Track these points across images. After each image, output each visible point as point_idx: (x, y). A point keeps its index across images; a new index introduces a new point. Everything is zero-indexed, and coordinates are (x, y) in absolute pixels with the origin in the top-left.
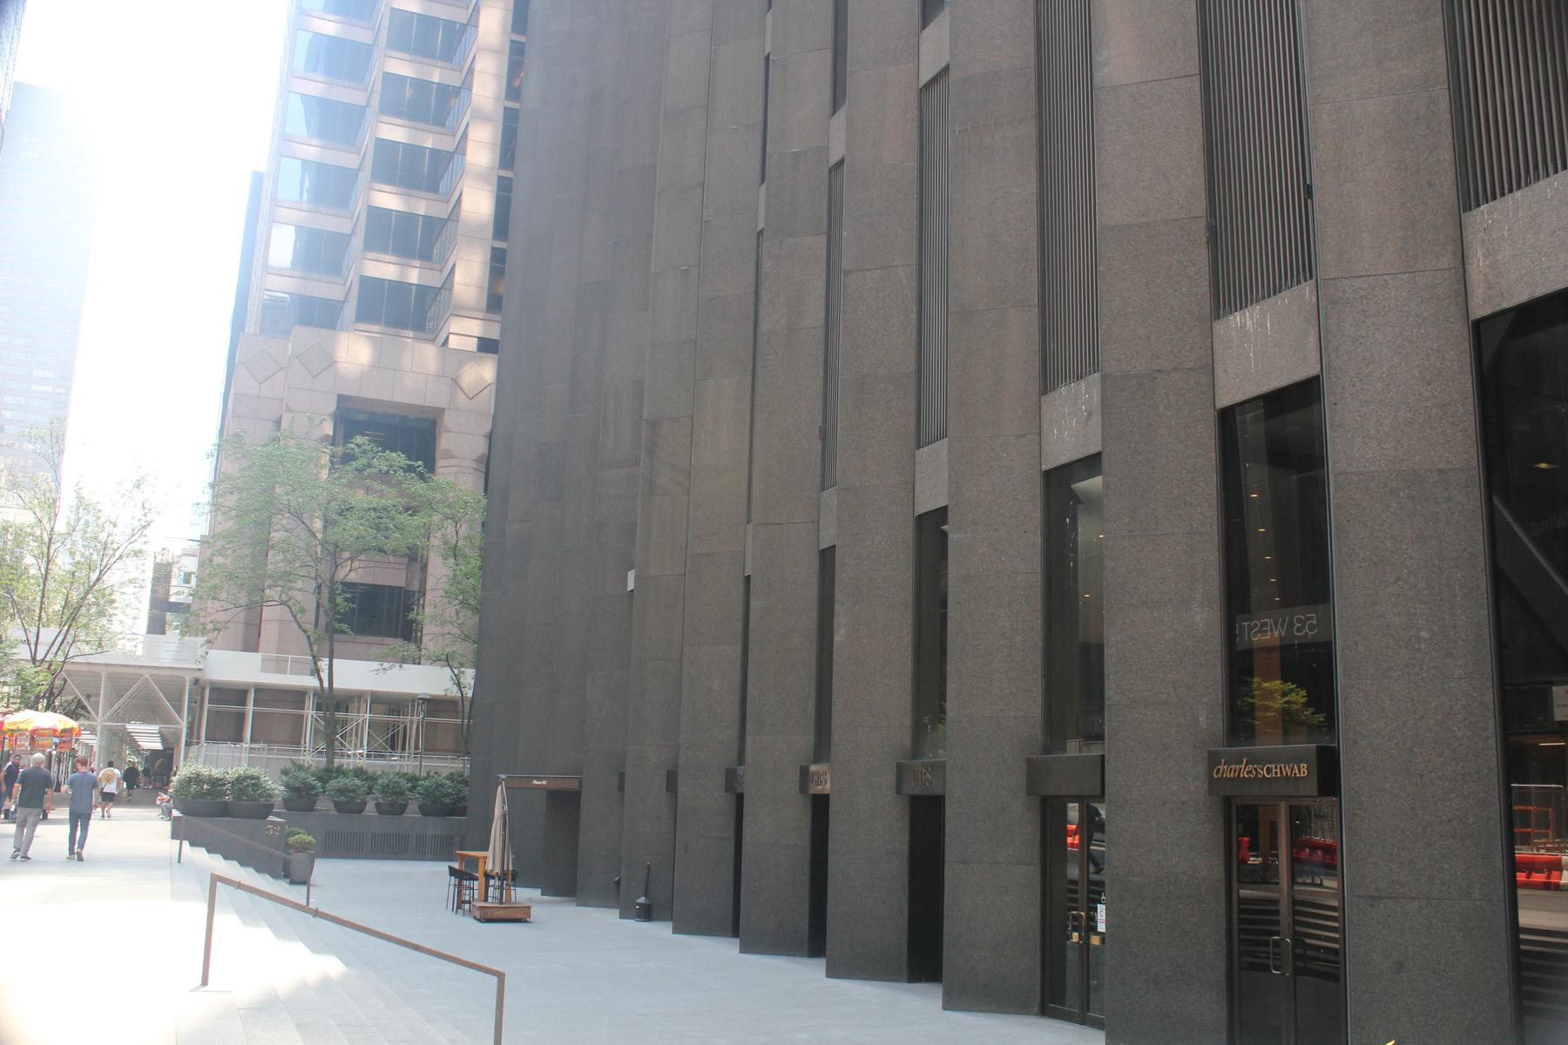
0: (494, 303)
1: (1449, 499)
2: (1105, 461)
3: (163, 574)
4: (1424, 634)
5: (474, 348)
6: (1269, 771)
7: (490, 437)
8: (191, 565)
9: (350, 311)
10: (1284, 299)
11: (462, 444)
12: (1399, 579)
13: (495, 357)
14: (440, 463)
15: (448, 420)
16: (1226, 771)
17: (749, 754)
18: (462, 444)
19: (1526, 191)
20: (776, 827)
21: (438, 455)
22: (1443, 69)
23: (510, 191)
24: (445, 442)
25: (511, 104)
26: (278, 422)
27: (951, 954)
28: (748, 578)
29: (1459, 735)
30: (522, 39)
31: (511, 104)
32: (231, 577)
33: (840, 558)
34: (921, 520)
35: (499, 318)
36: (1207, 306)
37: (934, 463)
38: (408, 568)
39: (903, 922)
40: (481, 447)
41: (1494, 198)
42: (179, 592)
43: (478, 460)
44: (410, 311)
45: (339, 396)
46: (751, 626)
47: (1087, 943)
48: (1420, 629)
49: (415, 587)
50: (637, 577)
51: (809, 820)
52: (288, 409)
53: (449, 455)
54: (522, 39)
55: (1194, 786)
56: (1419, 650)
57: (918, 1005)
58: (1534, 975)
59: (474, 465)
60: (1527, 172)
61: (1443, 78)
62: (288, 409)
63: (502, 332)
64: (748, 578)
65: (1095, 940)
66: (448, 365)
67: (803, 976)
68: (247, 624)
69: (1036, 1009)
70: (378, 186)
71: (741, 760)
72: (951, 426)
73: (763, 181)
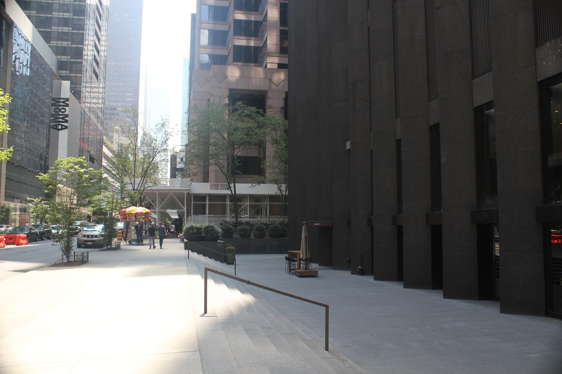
3: (174, 158)
7: (286, 99)
9: (231, 58)
11: (275, 103)
13: (287, 70)
15: (269, 94)
20: (417, 239)
21: (266, 108)
24: (269, 102)
26: (209, 100)
28: (372, 151)
30: (286, 28)
34: (431, 127)
35: (287, 55)
40: (281, 103)
43: (281, 108)
45: (231, 90)
50: (351, 144)
52: (212, 95)
53: (271, 107)
62: (212, 95)
68: (204, 173)
71: (400, 209)
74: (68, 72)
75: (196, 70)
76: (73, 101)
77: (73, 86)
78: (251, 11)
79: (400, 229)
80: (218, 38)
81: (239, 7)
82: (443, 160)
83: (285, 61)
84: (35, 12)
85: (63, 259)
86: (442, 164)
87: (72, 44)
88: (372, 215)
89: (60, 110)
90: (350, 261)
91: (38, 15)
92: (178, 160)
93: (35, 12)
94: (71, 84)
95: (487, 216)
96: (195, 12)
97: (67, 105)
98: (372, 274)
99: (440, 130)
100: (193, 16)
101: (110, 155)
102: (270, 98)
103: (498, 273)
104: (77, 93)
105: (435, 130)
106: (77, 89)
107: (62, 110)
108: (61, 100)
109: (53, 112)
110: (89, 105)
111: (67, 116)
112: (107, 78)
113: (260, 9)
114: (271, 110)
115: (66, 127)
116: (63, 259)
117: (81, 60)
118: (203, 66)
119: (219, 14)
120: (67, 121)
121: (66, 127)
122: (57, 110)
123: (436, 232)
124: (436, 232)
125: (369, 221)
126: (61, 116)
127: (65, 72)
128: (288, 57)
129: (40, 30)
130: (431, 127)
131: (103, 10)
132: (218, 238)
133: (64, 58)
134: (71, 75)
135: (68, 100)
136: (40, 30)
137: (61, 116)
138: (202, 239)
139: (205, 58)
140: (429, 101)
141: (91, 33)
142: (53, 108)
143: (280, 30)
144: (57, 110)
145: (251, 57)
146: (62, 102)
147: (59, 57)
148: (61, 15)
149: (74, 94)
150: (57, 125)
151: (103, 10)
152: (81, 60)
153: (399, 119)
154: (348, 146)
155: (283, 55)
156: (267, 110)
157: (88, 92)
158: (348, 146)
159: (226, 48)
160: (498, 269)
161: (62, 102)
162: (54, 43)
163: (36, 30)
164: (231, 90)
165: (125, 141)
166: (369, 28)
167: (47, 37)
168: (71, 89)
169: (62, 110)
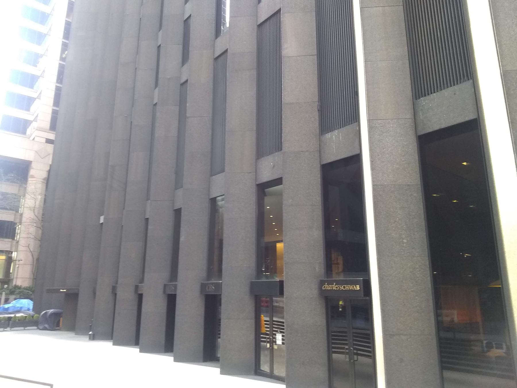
1: (411, 195)
2: (284, 181)
4: (405, 241)
5: (44, 142)
6: (344, 287)
7: (49, 172)
10: (345, 129)
11: (38, 173)
12: (396, 222)
14: (29, 179)
15: (33, 165)
16: (327, 287)
19: (438, 93)
20: (154, 307)
21: (29, 176)
22: (407, 53)
23: (57, 114)
24: (32, 172)
25: (58, 85)
28: (147, 219)
29: (418, 276)
30: (57, 109)
31: (58, 85)
32: (20, 186)
33: (183, 213)
34: (211, 199)
35: (55, 133)
36: (318, 131)
37: (219, 180)
38: (15, 215)
40: (44, 175)
41: (425, 96)
43: (44, 179)
44: (21, 127)
46: (148, 235)
47: (273, 348)
48: (403, 239)
49: (17, 221)
50: (105, 219)
51: (202, 340)
53: (33, 177)
54: (57, 109)
55: (315, 292)
56: (403, 246)
57: (210, 373)
58: (458, 367)
59: (42, 181)
60: (437, 87)
61: (407, 56)
63: (56, 138)
65: (275, 347)
67: (165, 361)
69: (253, 372)
71: (142, 281)
72: (226, 169)
73: (156, 85)
79: (140, 297)
86: (181, 242)
95: (213, 288)
102: (33, 177)
112: (119, 293)
113: (35, 87)
128: (56, 134)
140: (176, 189)
143: (53, 109)
153: (149, 201)
154: (102, 220)
158: (102, 220)
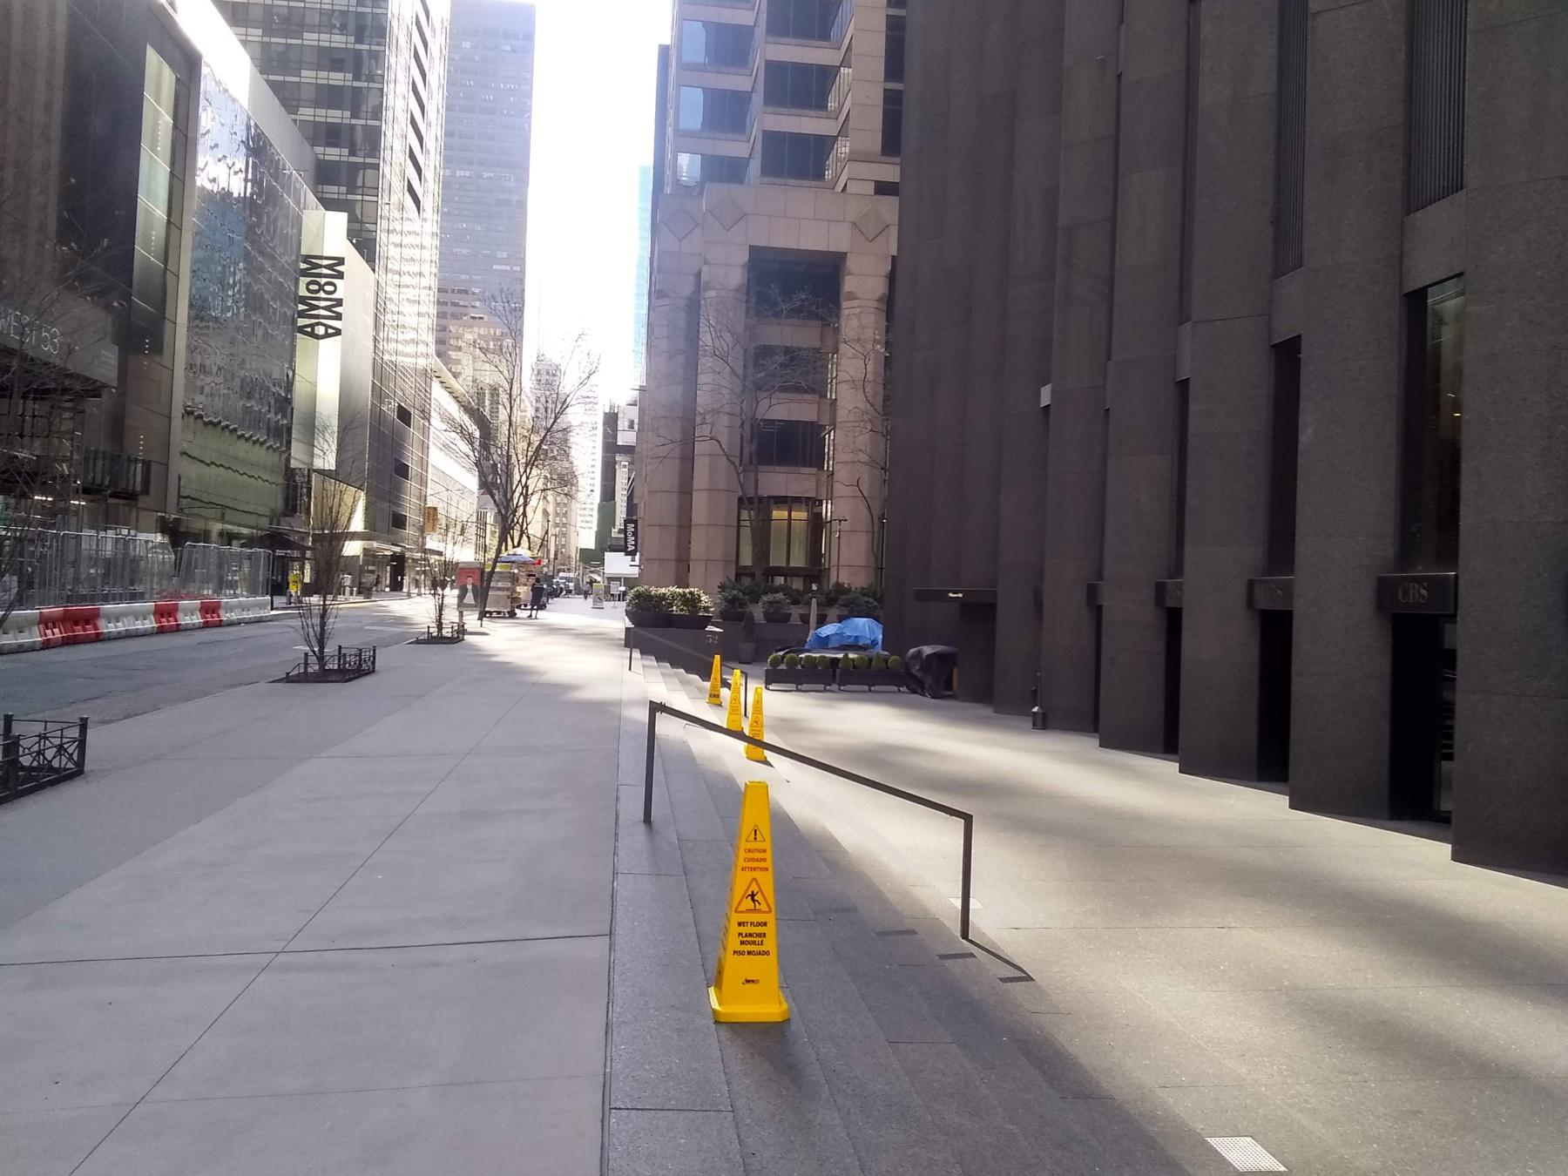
0: (892, 143)
3: (611, 420)
7: (892, 277)
8: (634, 413)
9: (755, 167)
11: (864, 283)
13: (896, 199)
15: (851, 263)
17: (1188, 564)
18: (864, 283)
20: (1219, 646)
24: (849, 284)
26: (699, 275)
27: (1458, 775)
28: (1184, 385)
30: (902, 13)
35: (897, 160)
39: (1384, 755)
40: (878, 287)
42: (626, 438)
45: (753, 250)
49: (825, 421)
50: (1053, 392)
52: (706, 262)
54: (902, 13)
59: (876, 304)
62: (706, 262)
64: (1184, 385)
66: (844, 217)
68: (683, 459)
70: (761, 468)
71: (1177, 568)
74: (343, 189)
75: (670, 206)
76: (354, 262)
77: (357, 226)
78: (811, 37)
79: (1174, 619)
80: (726, 112)
81: (780, 27)
82: (1305, 437)
83: (891, 173)
84: (260, 32)
85: (306, 664)
86: (1300, 447)
87: (352, 117)
88: (1101, 578)
89: (321, 288)
90: (1035, 692)
91: (266, 39)
92: (622, 424)
93: (260, 32)
94: (349, 221)
95: (1424, 592)
96: (667, 41)
97: (340, 275)
98: (1096, 730)
99: (1302, 356)
100: (664, 52)
101: (454, 409)
103: (1451, 747)
104: (365, 244)
105: (1287, 355)
106: (365, 235)
107: (328, 288)
108: (325, 262)
109: (303, 292)
110: (396, 277)
111: (339, 302)
114: (855, 303)
115: (338, 332)
116: (306, 664)
117: (374, 161)
118: (684, 190)
119: (729, 46)
120: (338, 317)
121: (338, 332)
122: (313, 287)
123: (1275, 631)
124: (1275, 631)
125: (1092, 593)
126: (323, 304)
127: (334, 189)
129: (272, 78)
130: (1408, 295)
131: (434, 31)
132: (708, 620)
133: (333, 154)
134: (350, 197)
135: (341, 261)
136: (272, 78)
137: (323, 304)
138: (669, 621)
139: (687, 165)
141: (403, 88)
142: (303, 281)
144: (313, 287)
145: (801, 160)
146: (326, 267)
147: (319, 150)
148: (325, 40)
149: (358, 247)
150: (312, 326)
151: (434, 31)
152: (374, 161)
153: (1188, 326)
154: (1046, 396)
155: (890, 159)
156: (845, 304)
157: (396, 245)
158: (1046, 396)
159: (745, 138)
160: (1450, 737)
161: (326, 267)
162: (306, 113)
163: (261, 79)
164: (753, 250)
165: (489, 376)
166: (1120, 76)
167: (287, 97)
168: (351, 234)
169: (328, 288)
